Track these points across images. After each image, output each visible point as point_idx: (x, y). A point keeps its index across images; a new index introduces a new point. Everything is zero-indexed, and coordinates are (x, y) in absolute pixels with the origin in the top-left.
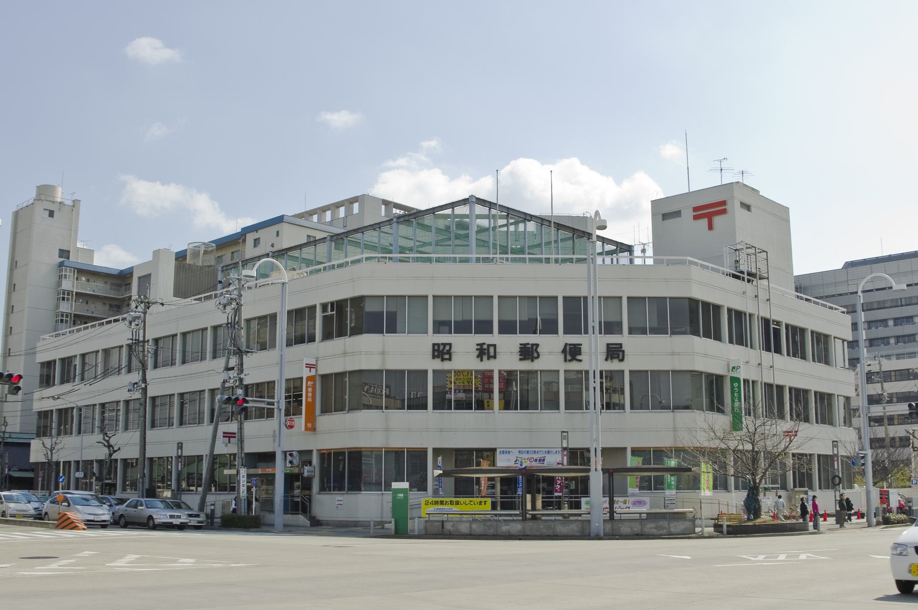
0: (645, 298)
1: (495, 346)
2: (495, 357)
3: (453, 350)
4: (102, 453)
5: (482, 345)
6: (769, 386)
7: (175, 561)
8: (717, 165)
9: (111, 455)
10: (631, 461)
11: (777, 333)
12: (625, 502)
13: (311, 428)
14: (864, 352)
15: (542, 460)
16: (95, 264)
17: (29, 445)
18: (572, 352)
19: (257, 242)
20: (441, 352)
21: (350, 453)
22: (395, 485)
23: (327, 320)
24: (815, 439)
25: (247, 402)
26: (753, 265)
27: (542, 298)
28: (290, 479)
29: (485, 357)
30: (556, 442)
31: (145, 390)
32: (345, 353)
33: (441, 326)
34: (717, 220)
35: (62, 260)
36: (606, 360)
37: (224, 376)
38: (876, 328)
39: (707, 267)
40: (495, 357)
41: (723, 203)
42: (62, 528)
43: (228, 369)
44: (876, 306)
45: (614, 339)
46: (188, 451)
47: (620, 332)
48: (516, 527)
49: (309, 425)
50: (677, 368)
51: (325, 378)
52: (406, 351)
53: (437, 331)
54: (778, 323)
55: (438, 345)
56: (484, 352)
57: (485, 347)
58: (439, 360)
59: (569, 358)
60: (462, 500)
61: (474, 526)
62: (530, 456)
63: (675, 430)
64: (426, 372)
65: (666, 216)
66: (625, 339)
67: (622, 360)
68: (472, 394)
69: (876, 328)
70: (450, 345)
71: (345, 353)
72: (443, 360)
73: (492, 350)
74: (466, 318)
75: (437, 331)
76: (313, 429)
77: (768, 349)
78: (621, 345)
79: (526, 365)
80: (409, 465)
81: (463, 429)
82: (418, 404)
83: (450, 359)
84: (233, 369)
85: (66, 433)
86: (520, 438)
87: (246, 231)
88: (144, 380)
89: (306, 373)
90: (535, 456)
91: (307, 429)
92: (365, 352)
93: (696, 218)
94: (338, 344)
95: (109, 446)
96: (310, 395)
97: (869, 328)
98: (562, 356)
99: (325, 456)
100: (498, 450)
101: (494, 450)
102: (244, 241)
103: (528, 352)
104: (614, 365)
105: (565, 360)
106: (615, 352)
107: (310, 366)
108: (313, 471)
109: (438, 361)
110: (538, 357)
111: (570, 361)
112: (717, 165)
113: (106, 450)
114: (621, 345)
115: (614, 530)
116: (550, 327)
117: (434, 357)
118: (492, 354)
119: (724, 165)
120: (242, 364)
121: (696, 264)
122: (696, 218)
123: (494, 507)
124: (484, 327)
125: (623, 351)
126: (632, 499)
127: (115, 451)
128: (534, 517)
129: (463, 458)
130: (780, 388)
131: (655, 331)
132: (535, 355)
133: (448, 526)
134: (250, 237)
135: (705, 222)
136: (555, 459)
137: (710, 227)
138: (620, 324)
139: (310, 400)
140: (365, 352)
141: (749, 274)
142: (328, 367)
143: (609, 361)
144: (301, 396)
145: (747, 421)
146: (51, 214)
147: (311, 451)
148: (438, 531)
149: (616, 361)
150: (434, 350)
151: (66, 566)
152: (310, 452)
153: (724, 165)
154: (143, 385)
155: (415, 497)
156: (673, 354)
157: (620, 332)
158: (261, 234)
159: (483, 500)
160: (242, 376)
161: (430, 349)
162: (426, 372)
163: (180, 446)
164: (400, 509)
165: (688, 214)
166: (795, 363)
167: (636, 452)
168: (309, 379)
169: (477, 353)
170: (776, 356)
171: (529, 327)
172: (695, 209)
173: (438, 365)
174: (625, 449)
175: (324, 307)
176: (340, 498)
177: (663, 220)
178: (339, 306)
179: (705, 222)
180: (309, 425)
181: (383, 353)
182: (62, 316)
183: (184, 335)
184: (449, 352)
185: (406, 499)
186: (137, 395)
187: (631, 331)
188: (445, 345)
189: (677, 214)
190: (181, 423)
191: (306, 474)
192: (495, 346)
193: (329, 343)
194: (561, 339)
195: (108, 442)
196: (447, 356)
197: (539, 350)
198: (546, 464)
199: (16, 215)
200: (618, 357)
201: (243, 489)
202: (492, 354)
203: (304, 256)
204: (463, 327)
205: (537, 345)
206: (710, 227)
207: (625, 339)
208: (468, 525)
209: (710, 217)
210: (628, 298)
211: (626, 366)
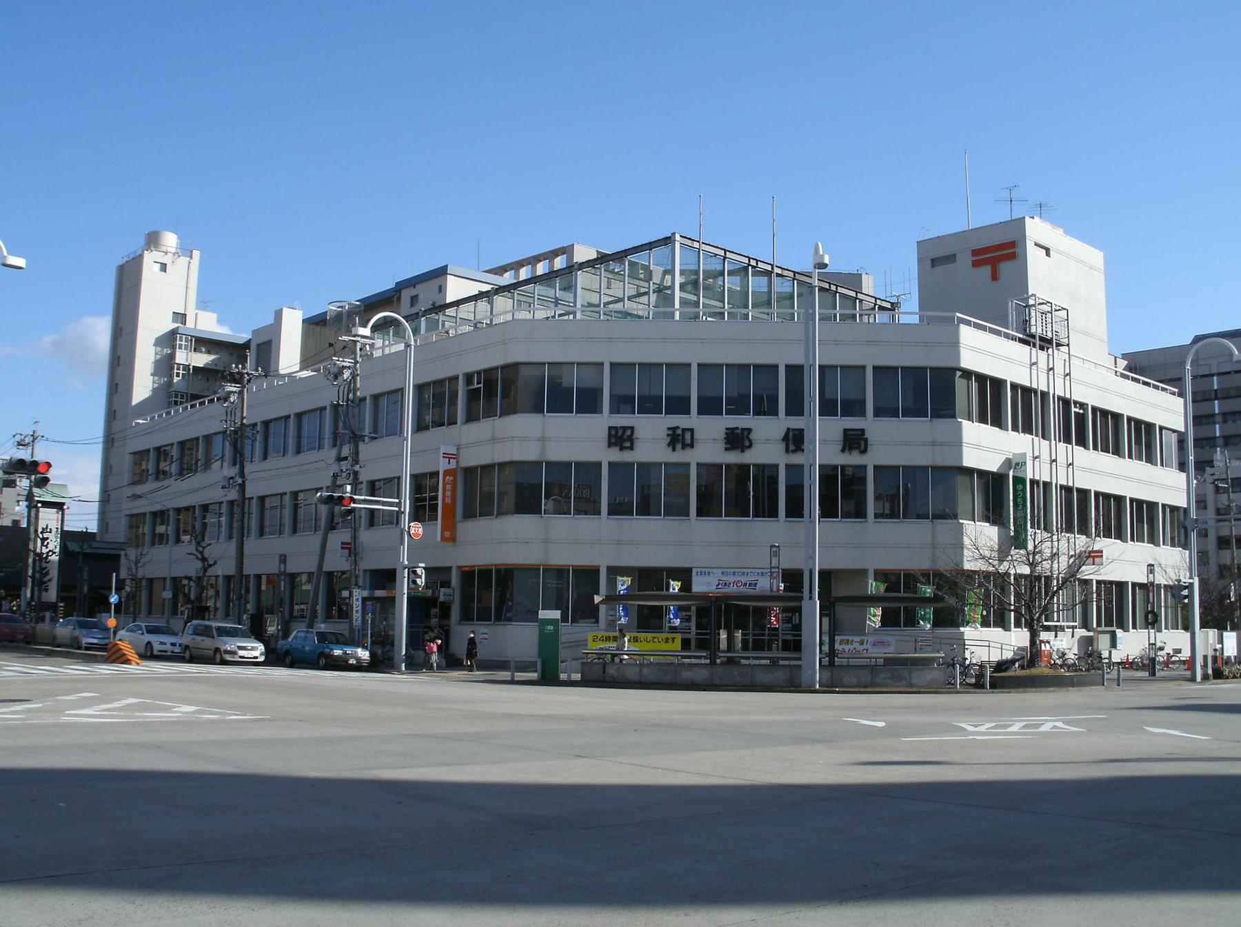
0: (896, 368)
1: (692, 430)
2: (692, 446)
3: (636, 435)
4: (192, 568)
5: (674, 429)
6: (1067, 490)
7: (168, 709)
8: (1006, 195)
9: (205, 570)
10: (873, 587)
11: (1081, 419)
12: (862, 643)
13: (450, 537)
14: (1218, 455)
15: (753, 585)
16: (996, 528)
17: (118, 557)
18: (795, 440)
19: (414, 300)
20: (620, 438)
21: (498, 571)
22: (544, 614)
23: (473, 395)
24: (1125, 560)
25: (352, 500)
26: (1049, 329)
27: (757, 367)
28: (418, 604)
29: (679, 446)
30: (761, 559)
31: (242, 487)
32: (493, 439)
33: (622, 403)
34: (1004, 267)
35: (176, 325)
36: (843, 451)
37: (335, 468)
38: (1234, 421)
39: (983, 328)
40: (692, 446)
41: (1012, 244)
42: (113, 662)
43: (340, 459)
44: (1233, 393)
45: (853, 423)
46: (291, 568)
47: (862, 413)
48: (702, 675)
49: (447, 534)
50: (939, 463)
51: (469, 472)
52: (576, 438)
53: (615, 409)
54: (1082, 406)
55: (616, 428)
56: (677, 439)
57: (679, 432)
58: (617, 449)
59: (792, 447)
60: (642, 635)
61: (645, 671)
62: (737, 578)
63: (934, 546)
64: (599, 464)
65: (935, 262)
66: (870, 424)
67: (864, 451)
68: (642, 494)
69: (1234, 421)
70: (632, 428)
71: (493, 439)
72: (622, 449)
73: (688, 436)
74: (654, 392)
75: (615, 409)
76: (453, 539)
77: (1067, 440)
78: (863, 431)
79: (733, 458)
80: (577, 589)
81: (650, 541)
82: (588, 506)
83: (631, 448)
84: (346, 458)
85: (160, 543)
86: (725, 555)
87: (402, 286)
88: (242, 474)
89: (443, 465)
90: (744, 579)
91: (443, 538)
92: (524, 437)
93: (976, 264)
94: (483, 428)
95: (204, 559)
96: (448, 494)
97: (1225, 421)
98: (783, 446)
99: (468, 575)
100: (694, 571)
101: (689, 570)
102: (399, 299)
103: (737, 440)
104: (854, 459)
105: (787, 451)
106: (854, 441)
107: (448, 456)
108: (452, 594)
109: (615, 450)
110: (750, 446)
111: (793, 451)
112: (1006, 195)
113: (199, 564)
114: (863, 431)
115: (840, 677)
116: (766, 407)
117: (610, 445)
118: (688, 441)
119: (1015, 194)
120: (357, 453)
121: (968, 323)
122: (976, 264)
123: (686, 644)
124: (679, 405)
125: (866, 440)
126: (871, 639)
127: (210, 566)
128: (731, 661)
129: (650, 578)
130: (1084, 493)
131: (911, 412)
132: (747, 443)
133: (611, 671)
134: (406, 295)
135: (986, 270)
136: (764, 584)
137: (995, 277)
138: (862, 403)
139: (448, 500)
140: (524, 437)
141: (1042, 339)
142: (474, 458)
143: (847, 453)
144: (436, 498)
145: (1034, 536)
146: (164, 267)
147: (450, 569)
148: (600, 676)
149: (855, 453)
150: (610, 436)
151: (108, 710)
152: (448, 569)
153: (1015, 194)
154: (240, 481)
155: (569, 632)
156: (933, 444)
157: (862, 413)
158: (419, 290)
159: (671, 636)
160: (357, 468)
161: (604, 434)
162: (599, 464)
163: (283, 559)
164: (549, 647)
165: (965, 259)
166: (1106, 461)
167: (881, 575)
168: (447, 473)
169: (668, 439)
170: (1079, 450)
171: (739, 406)
172: (975, 252)
173: (615, 455)
174: (865, 571)
175: (469, 378)
176: (486, 631)
177: (933, 266)
178: (488, 376)
179: (986, 270)
180: (447, 534)
181: (543, 439)
182: (176, 396)
183: (299, 416)
184: (631, 439)
185: (556, 631)
186: (233, 495)
187: (878, 413)
188: (625, 428)
189: (951, 259)
190: (295, 530)
191: (442, 598)
192: (692, 430)
193: (473, 427)
194: (781, 423)
195: (202, 553)
196: (627, 444)
197: (752, 436)
198: (758, 590)
199: (122, 270)
200: (859, 447)
201: (357, 616)
202: (688, 441)
203: (461, 315)
204: (650, 405)
205: (750, 430)
206: (995, 277)
207: (870, 424)
208: (637, 669)
209: (994, 263)
210: (874, 368)
211: (870, 460)
